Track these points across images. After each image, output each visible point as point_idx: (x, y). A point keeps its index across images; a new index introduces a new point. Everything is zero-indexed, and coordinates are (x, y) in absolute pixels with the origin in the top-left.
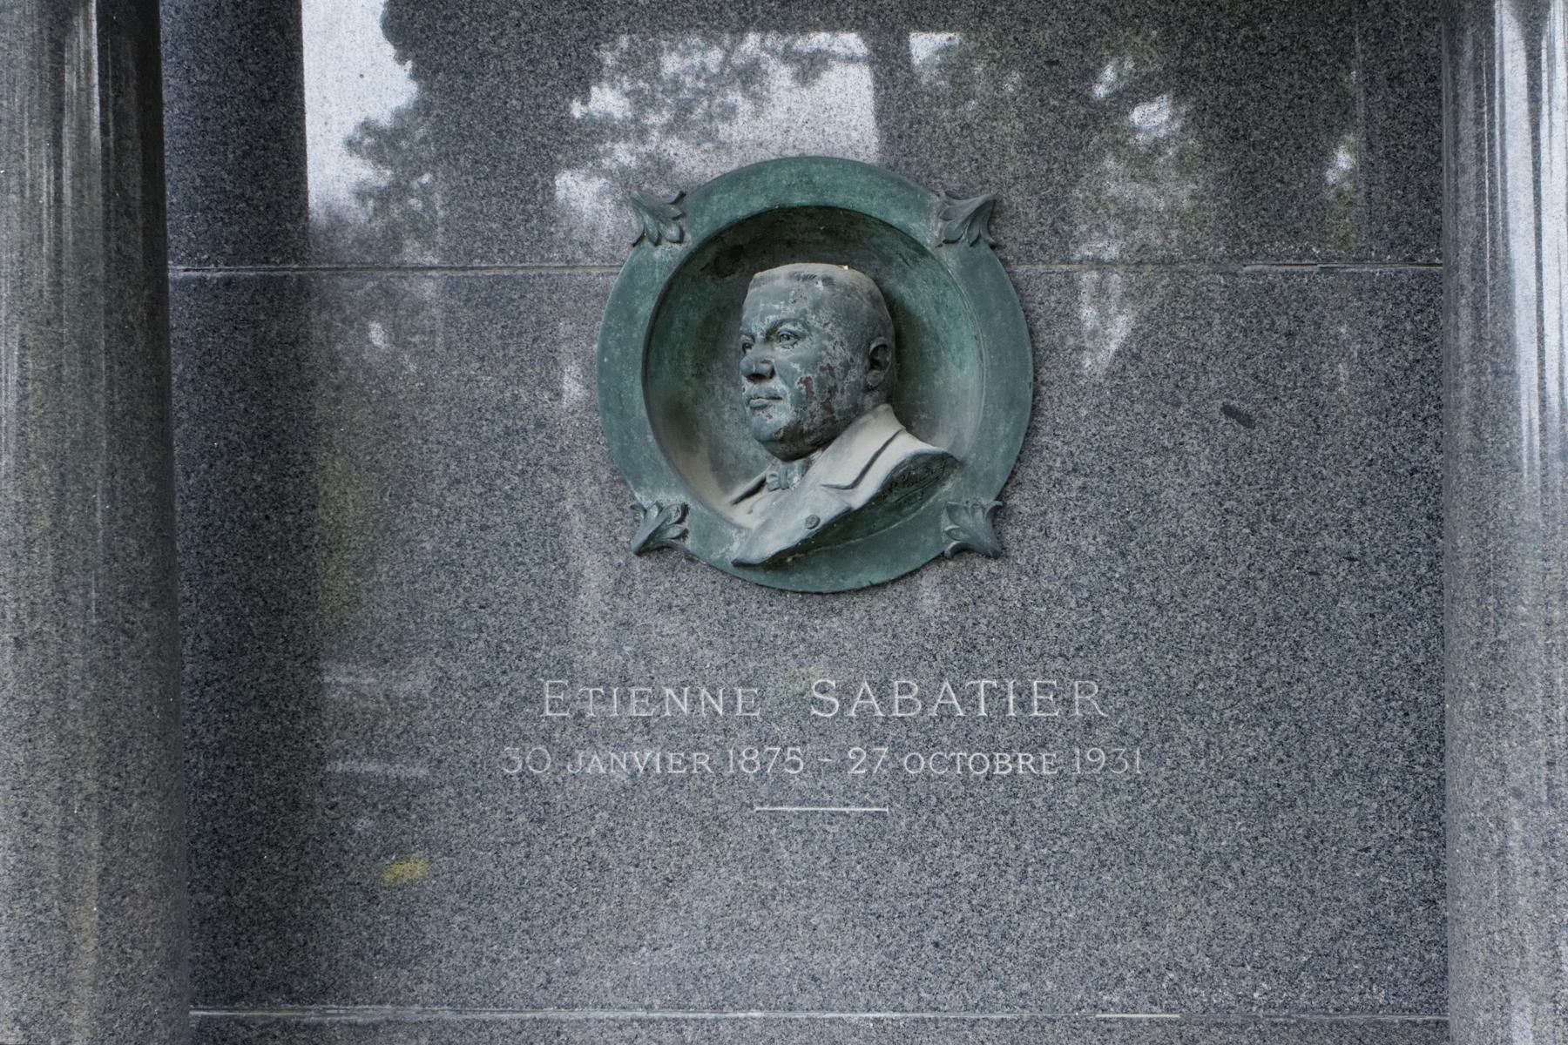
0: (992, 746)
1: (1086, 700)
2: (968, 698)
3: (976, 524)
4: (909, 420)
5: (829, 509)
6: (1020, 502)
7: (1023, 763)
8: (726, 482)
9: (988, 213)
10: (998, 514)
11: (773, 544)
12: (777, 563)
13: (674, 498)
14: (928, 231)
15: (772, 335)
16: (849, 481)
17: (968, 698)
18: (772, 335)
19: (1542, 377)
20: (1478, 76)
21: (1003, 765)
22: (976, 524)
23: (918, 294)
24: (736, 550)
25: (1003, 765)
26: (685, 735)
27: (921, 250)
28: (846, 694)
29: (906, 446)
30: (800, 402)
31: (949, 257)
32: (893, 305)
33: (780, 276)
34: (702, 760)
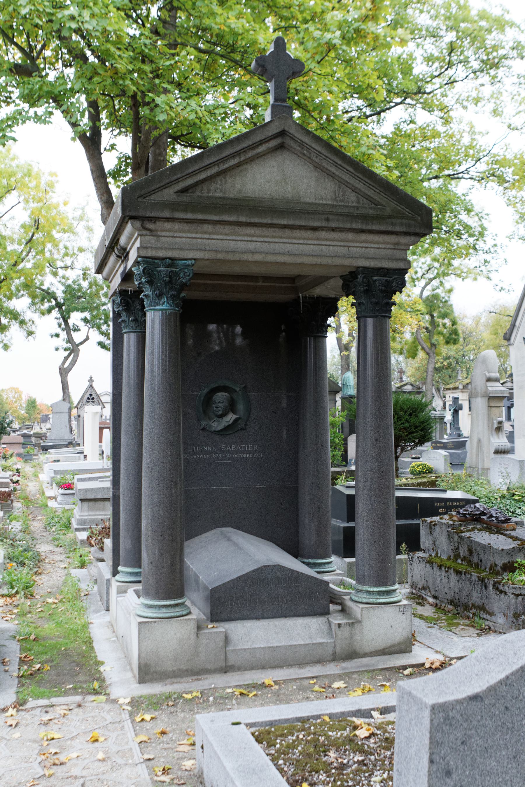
0: (244, 453)
1: (255, 448)
2: (241, 448)
3: (243, 426)
4: (234, 412)
5: (227, 424)
6: (248, 423)
7: (248, 455)
8: (210, 420)
9: (245, 387)
10: (246, 425)
11: (219, 428)
12: (219, 431)
13: (206, 423)
14: (237, 389)
15: (219, 402)
16: (70, 377)
17: (241, 448)
18: (219, 402)
19: (340, 246)
20: (301, 153)
21: (245, 456)
22: (243, 426)
23: (235, 396)
24: (213, 429)
25: (245, 456)
26: (207, 452)
27: (236, 391)
28: (226, 447)
29: (235, 417)
30: (223, 411)
31: (240, 393)
32: (232, 398)
33: (220, 394)
34: (208, 456)
